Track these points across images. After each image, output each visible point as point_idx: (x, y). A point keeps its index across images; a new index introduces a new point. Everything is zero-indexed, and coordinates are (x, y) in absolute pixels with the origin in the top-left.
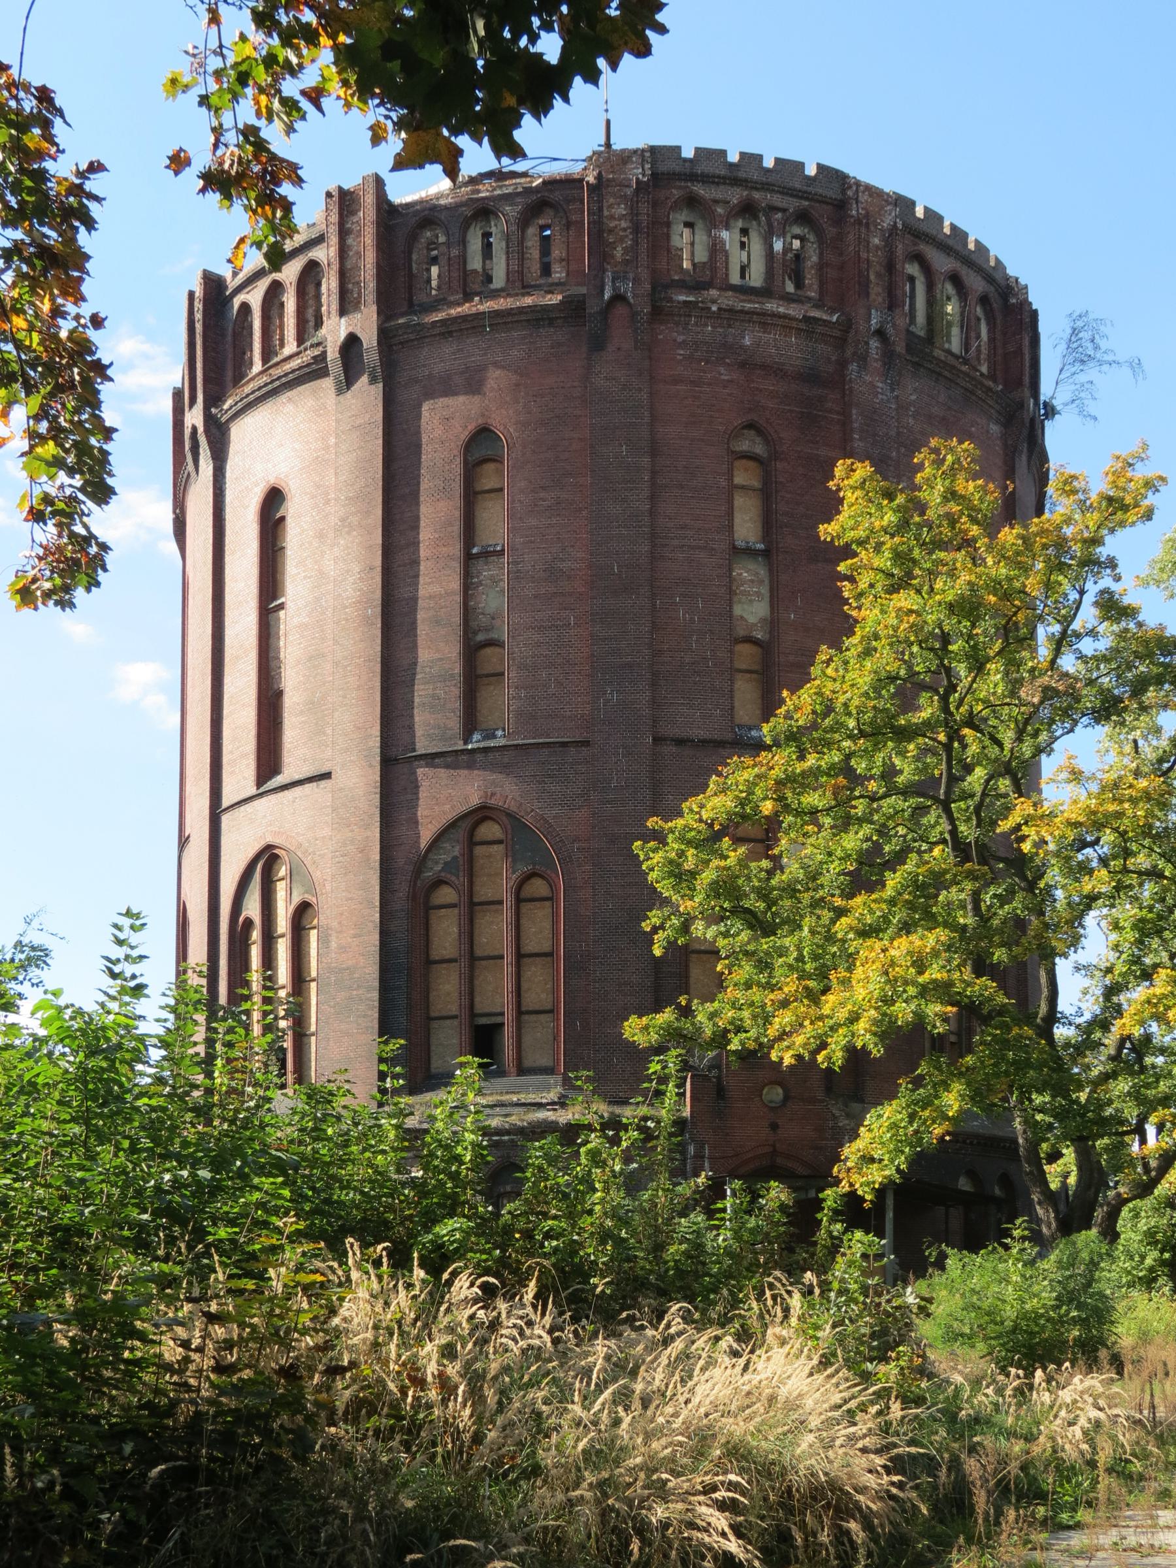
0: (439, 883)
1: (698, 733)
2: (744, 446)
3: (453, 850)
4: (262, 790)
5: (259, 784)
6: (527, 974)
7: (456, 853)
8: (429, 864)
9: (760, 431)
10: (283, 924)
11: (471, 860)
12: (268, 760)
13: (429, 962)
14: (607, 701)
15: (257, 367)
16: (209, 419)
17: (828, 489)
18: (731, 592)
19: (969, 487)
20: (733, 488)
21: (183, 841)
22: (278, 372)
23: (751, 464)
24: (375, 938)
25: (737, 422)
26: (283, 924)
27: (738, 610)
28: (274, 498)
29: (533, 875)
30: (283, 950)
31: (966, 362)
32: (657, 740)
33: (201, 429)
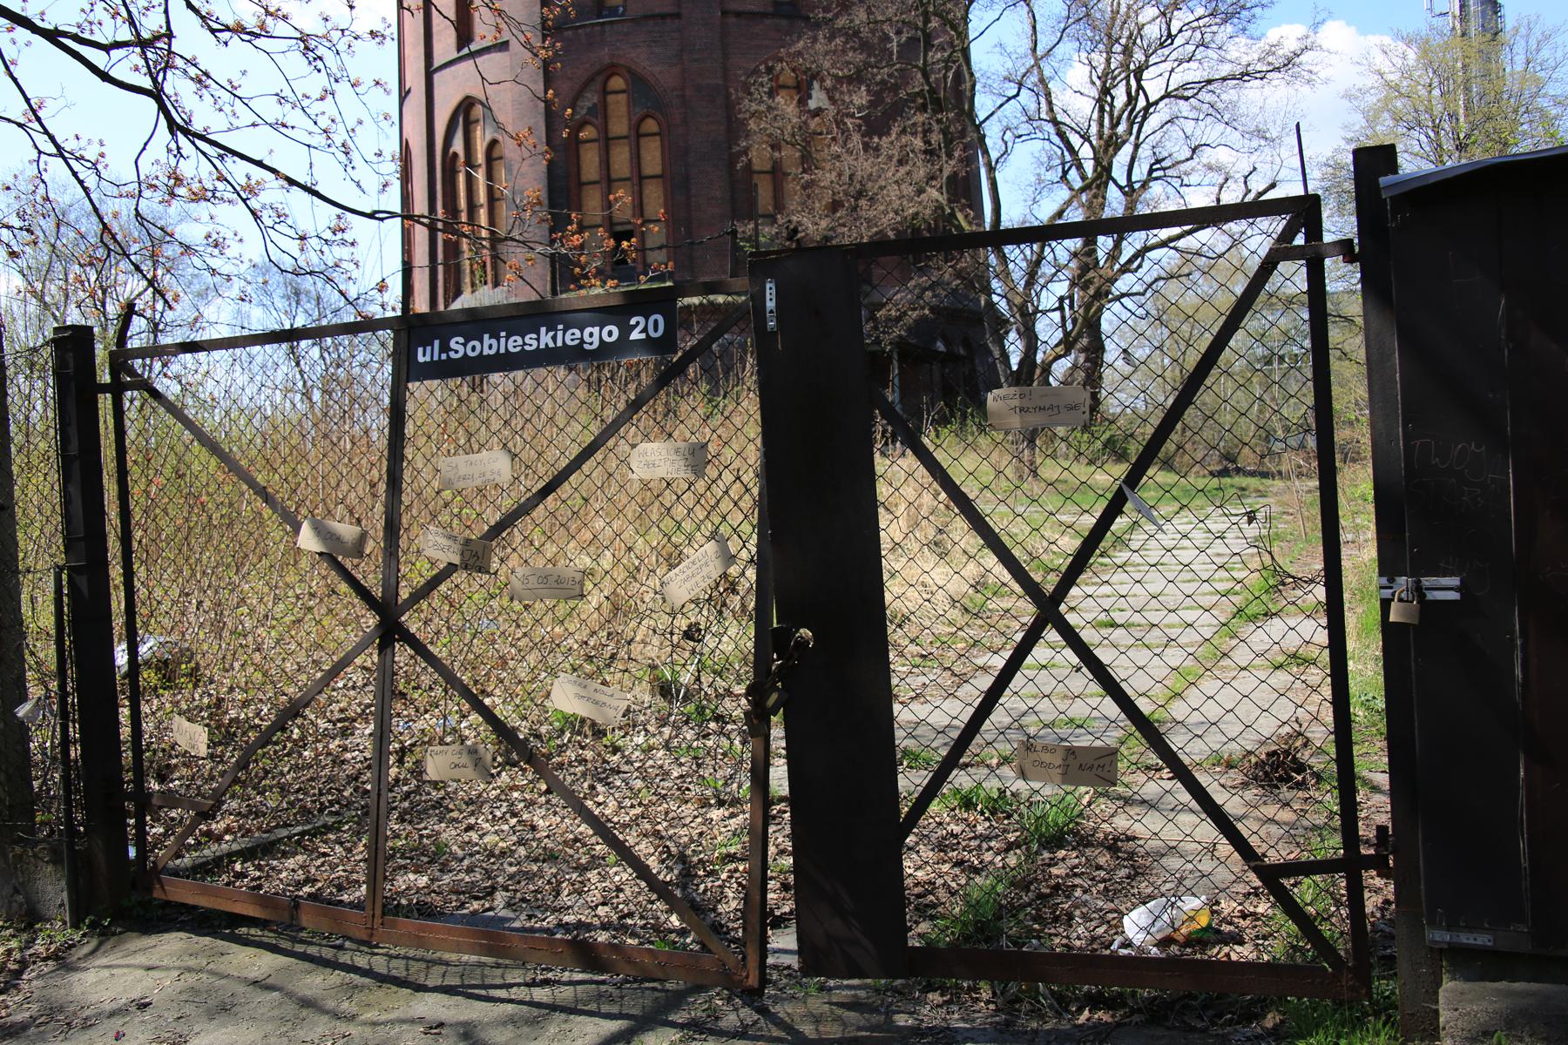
3: (160, 79)
4: (465, 51)
5: (459, 50)
6: (646, 192)
10: (480, 158)
12: (464, 33)
13: (581, 184)
26: (480, 158)
29: (647, 116)
32: (724, 13)
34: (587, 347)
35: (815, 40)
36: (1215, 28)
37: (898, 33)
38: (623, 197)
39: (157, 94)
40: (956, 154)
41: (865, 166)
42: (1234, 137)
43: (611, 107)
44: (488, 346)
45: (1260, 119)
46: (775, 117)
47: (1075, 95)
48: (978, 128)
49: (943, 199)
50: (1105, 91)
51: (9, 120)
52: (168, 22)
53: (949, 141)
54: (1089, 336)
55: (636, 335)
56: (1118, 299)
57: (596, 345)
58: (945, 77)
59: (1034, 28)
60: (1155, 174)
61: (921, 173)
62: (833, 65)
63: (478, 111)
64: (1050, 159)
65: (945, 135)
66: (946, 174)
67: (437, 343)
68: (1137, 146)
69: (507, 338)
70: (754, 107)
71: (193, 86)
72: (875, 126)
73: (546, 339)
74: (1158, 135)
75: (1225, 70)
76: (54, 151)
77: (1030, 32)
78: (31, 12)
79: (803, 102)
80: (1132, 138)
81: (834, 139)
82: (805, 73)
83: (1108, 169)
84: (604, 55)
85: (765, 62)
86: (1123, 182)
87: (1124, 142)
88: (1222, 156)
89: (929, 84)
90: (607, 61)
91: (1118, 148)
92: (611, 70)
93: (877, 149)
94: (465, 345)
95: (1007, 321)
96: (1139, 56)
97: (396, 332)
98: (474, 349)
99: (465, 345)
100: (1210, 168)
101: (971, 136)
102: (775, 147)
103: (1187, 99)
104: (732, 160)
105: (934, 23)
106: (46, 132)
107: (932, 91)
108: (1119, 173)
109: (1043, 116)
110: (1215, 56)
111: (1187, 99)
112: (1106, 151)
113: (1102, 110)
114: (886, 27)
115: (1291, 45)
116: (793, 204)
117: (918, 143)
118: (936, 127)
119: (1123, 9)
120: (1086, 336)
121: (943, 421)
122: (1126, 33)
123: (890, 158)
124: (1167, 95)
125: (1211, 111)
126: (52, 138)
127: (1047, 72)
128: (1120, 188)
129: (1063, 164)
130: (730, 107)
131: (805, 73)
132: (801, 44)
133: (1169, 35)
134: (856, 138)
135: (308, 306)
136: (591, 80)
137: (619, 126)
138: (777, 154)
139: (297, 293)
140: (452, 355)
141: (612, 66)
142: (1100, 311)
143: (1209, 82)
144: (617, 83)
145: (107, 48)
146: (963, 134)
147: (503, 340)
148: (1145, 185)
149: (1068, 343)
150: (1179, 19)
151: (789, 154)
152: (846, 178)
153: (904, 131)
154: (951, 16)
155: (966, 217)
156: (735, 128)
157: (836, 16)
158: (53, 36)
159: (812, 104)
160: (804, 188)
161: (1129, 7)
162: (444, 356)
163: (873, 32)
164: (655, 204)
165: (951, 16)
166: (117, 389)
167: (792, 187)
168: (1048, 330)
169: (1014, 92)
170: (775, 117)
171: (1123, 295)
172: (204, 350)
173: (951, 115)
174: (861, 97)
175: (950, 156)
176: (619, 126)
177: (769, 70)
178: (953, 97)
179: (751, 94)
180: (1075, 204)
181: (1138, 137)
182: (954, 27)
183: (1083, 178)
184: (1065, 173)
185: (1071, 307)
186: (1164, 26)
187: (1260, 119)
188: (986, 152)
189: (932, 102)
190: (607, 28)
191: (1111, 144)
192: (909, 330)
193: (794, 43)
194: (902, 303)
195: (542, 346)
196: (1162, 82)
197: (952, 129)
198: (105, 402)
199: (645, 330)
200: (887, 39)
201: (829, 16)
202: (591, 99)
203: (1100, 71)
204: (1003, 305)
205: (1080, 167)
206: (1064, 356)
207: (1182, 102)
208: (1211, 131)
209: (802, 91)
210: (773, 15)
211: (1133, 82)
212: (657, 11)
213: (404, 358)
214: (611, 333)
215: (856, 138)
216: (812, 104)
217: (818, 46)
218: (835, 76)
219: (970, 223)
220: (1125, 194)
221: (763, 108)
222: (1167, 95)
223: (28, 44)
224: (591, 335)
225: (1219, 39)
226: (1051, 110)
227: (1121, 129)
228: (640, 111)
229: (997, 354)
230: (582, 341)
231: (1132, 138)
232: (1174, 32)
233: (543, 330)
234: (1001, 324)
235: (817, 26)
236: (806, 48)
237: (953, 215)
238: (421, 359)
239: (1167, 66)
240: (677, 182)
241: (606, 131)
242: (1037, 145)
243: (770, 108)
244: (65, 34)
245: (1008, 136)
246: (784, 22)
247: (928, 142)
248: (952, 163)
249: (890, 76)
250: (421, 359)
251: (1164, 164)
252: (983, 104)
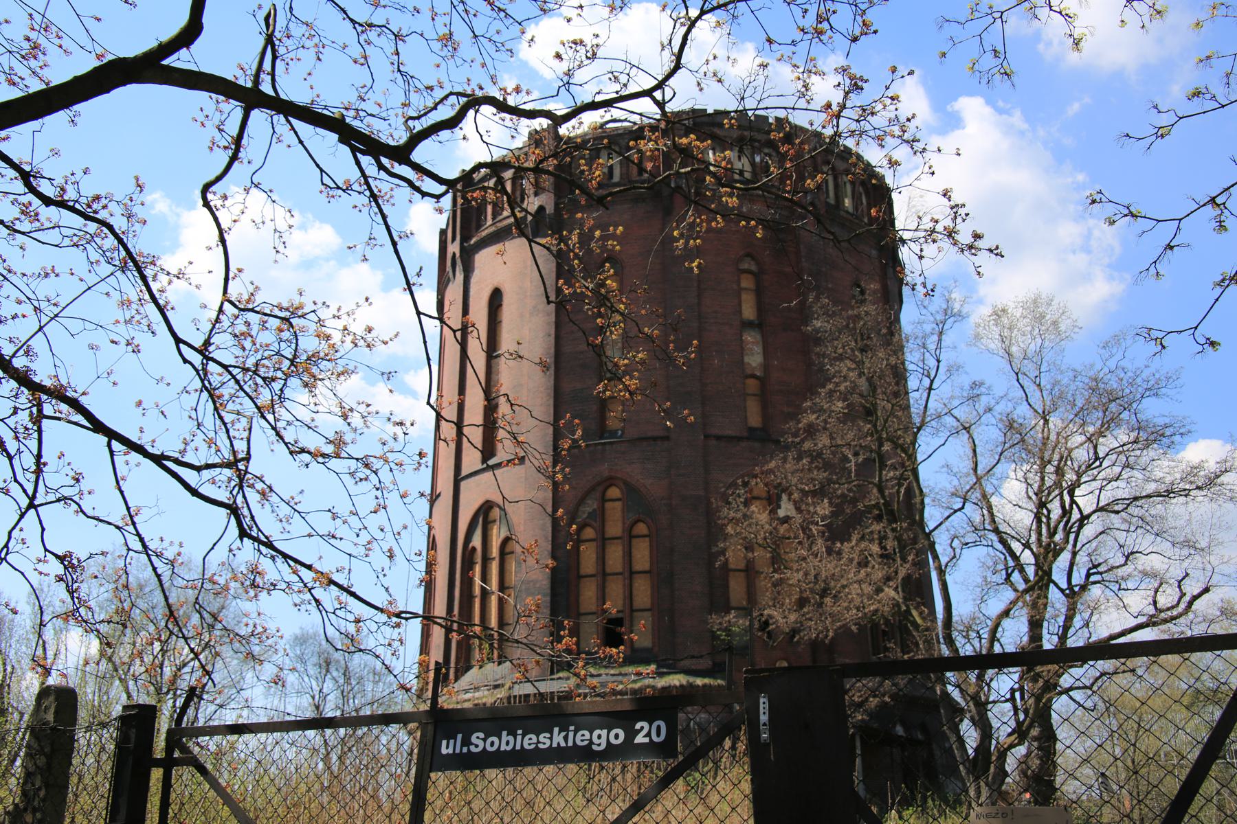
1: (729, 432)
2: (745, 266)
9: (753, 258)
10: (495, 552)
11: (603, 510)
12: (488, 450)
13: (580, 577)
15: (489, 222)
16: (462, 248)
17: (843, 686)
18: (742, 349)
20: (740, 290)
21: (429, 359)
22: (500, 225)
23: (750, 276)
25: (742, 253)
26: (495, 552)
27: (746, 359)
28: (496, 298)
30: (494, 568)
31: (857, 217)
32: (706, 437)
33: (458, 255)
34: (595, 747)
35: (785, 460)
36: (1138, 453)
37: (856, 454)
38: (616, 589)
39: (234, 510)
40: (910, 558)
41: (829, 567)
42: (1165, 546)
44: (505, 742)
45: (1187, 530)
46: (750, 525)
47: (1015, 511)
48: (928, 535)
49: (899, 598)
50: (1042, 505)
51: (110, 523)
52: (249, 448)
53: (902, 546)
54: (1040, 726)
55: (640, 739)
56: (1067, 691)
57: (603, 747)
58: (898, 492)
59: (974, 451)
60: (1092, 579)
61: (879, 574)
62: (800, 480)
63: (496, 513)
64: (996, 564)
65: (899, 542)
66: (901, 576)
67: (460, 736)
68: (1074, 554)
69: (523, 736)
70: (732, 514)
71: (258, 497)
72: (837, 533)
73: (558, 739)
74: (1094, 544)
75: (1151, 488)
76: (140, 548)
77: (971, 454)
78: (145, 441)
79: (773, 512)
80: (1070, 547)
81: (800, 543)
82: (776, 488)
83: (1049, 573)
84: (604, 470)
85: (742, 477)
86: (1064, 585)
87: (1062, 550)
88: (1154, 562)
89: (883, 497)
90: (606, 474)
91: (1057, 554)
92: (610, 482)
93: (839, 553)
94: (484, 740)
95: (963, 709)
96: (1070, 476)
97: (423, 726)
98: (492, 744)
99: (484, 740)
100: (1145, 574)
101: (922, 543)
102: (749, 548)
103: (1117, 512)
104: (712, 557)
105: (887, 447)
106: (138, 535)
107: (887, 504)
108: (1059, 576)
109: (988, 527)
110: (1141, 476)
111: (1117, 512)
112: (1045, 558)
113: (1039, 522)
114: (846, 451)
115: (1212, 466)
116: (765, 598)
117: (875, 548)
118: (890, 534)
119: (1053, 437)
120: (1037, 725)
121: (906, 803)
122: (1056, 457)
123: (851, 560)
124: (1099, 509)
125: (1140, 523)
126: (142, 540)
127: (989, 489)
128: (1062, 591)
129: (1007, 569)
130: (710, 515)
131: (776, 488)
132: (773, 464)
133: (1097, 458)
134: (820, 545)
135: (335, 674)
136: (593, 489)
137: (614, 528)
138: (750, 555)
139: (328, 664)
140: (473, 749)
141: (611, 478)
143: (1136, 499)
144: (614, 492)
145: (198, 469)
146: (915, 541)
147: (519, 738)
148: (1084, 588)
149: (1020, 733)
150: (1106, 444)
151: (761, 556)
152: (811, 577)
153: (862, 538)
154: (901, 441)
155: (921, 614)
156: (714, 531)
157: (803, 441)
158: (158, 460)
159: (781, 513)
160: (775, 585)
161: (1058, 434)
162: (465, 750)
163: (833, 453)
164: (643, 593)
165: (901, 441)
166: (168, 764)
167: (763, 584)
168: (1002, 718)
169: (960, 505)
170: (750, 525)
171: (1071, 689)
172: (251, 732)
173: (905, 525)
174: (824, 508)
175: (904, 560)
176: (614, 528)
177: (745, 484)
178: (905, 508)
179: (729, 503)
180: (1020, 604)
181: (1075, 545)
182: (904, 451)
183: (1026, 580)
184: (1009, 576)
185: (1022, 698)
186: (1091, 452)
187: (1187, 530)
188: (936, 557)
189: (888, 513)
190: (608, 447)
191: (1047, 554)
192: (871, 715)
193: (767, 462)
194: (865, 695)
195: (555, 745)
196: (1093, 499)
197: (905, 536)
198: (157, 774)
199: (648, 735)
200: (845, 459)
201: (797, 440)
202: (591, 505)
203: (1036, 486)
204: (956, 694)
205: (1022, 570)
206: (1019, 744)
207: (1113, 515)
208: (1144, 542)
209: (772, 502)
210: (748, 439)
211: (1067, 498)
212: (650, 434)
213: (429, 749)
214: (618, 736)
215: (820, 542)
216: (781, 513)
217: (788, 466)
218: (802, 491)
219: (924, 619)
220: (1066, 596)
221: (739, 515)
222: (1099, 509)
223: (138, 465)
224: (599, 737)
225: (1144, 460)
226: (994, 521)
227: (1058, 537)
229: (953, 739)
230: (591, 742)
231: (1070, 547)
232: (1101, 455)
233: (556, 730)
234: (957, 712)
235: (787, 448)
236: (778, 467)
237: (908, 612)
238: (444, 751)
239: (1097, 484)
240: (663, 577)
241: (603, 533)
242: (981, 551)
243: (745, 516)
244: (168, 458)
245: (956, 543)
246: (757, 445)
247: (883, 548)
248: (907, 566)
249: (849, 490)
250: (444, 751)
251: (1101, 569)
252: (932, 515)
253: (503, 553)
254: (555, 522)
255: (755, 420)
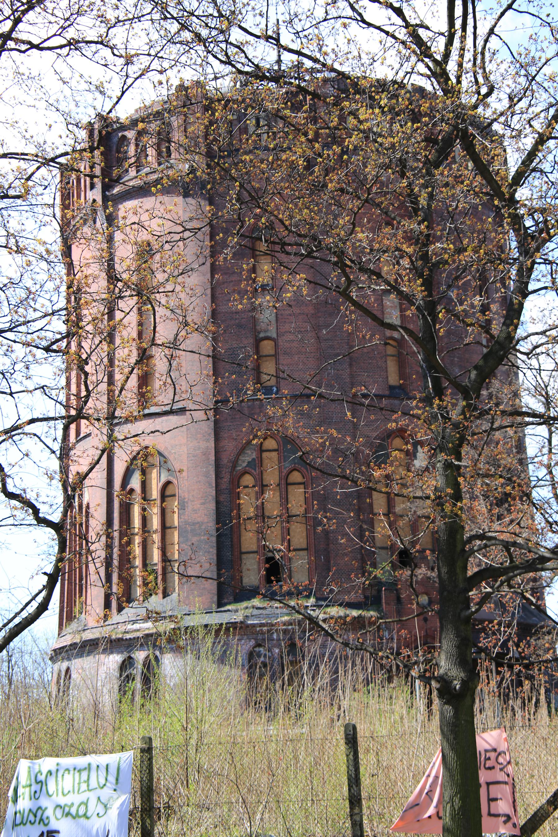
0: (245, 473)
7: (254, 457)
8: (240, 462)
10: (155, 493)
14: (329, 374)
19: (350, 146)
24: (212, 506)
26: (155, 493)
43: (265, 462)
137: (272, 476)
142: (515, 191)
164: (299, 534)
176: (272, 476)
228: (288, 465)
253: (163, 496)
254: (218, 503)
255: (394, 379)
